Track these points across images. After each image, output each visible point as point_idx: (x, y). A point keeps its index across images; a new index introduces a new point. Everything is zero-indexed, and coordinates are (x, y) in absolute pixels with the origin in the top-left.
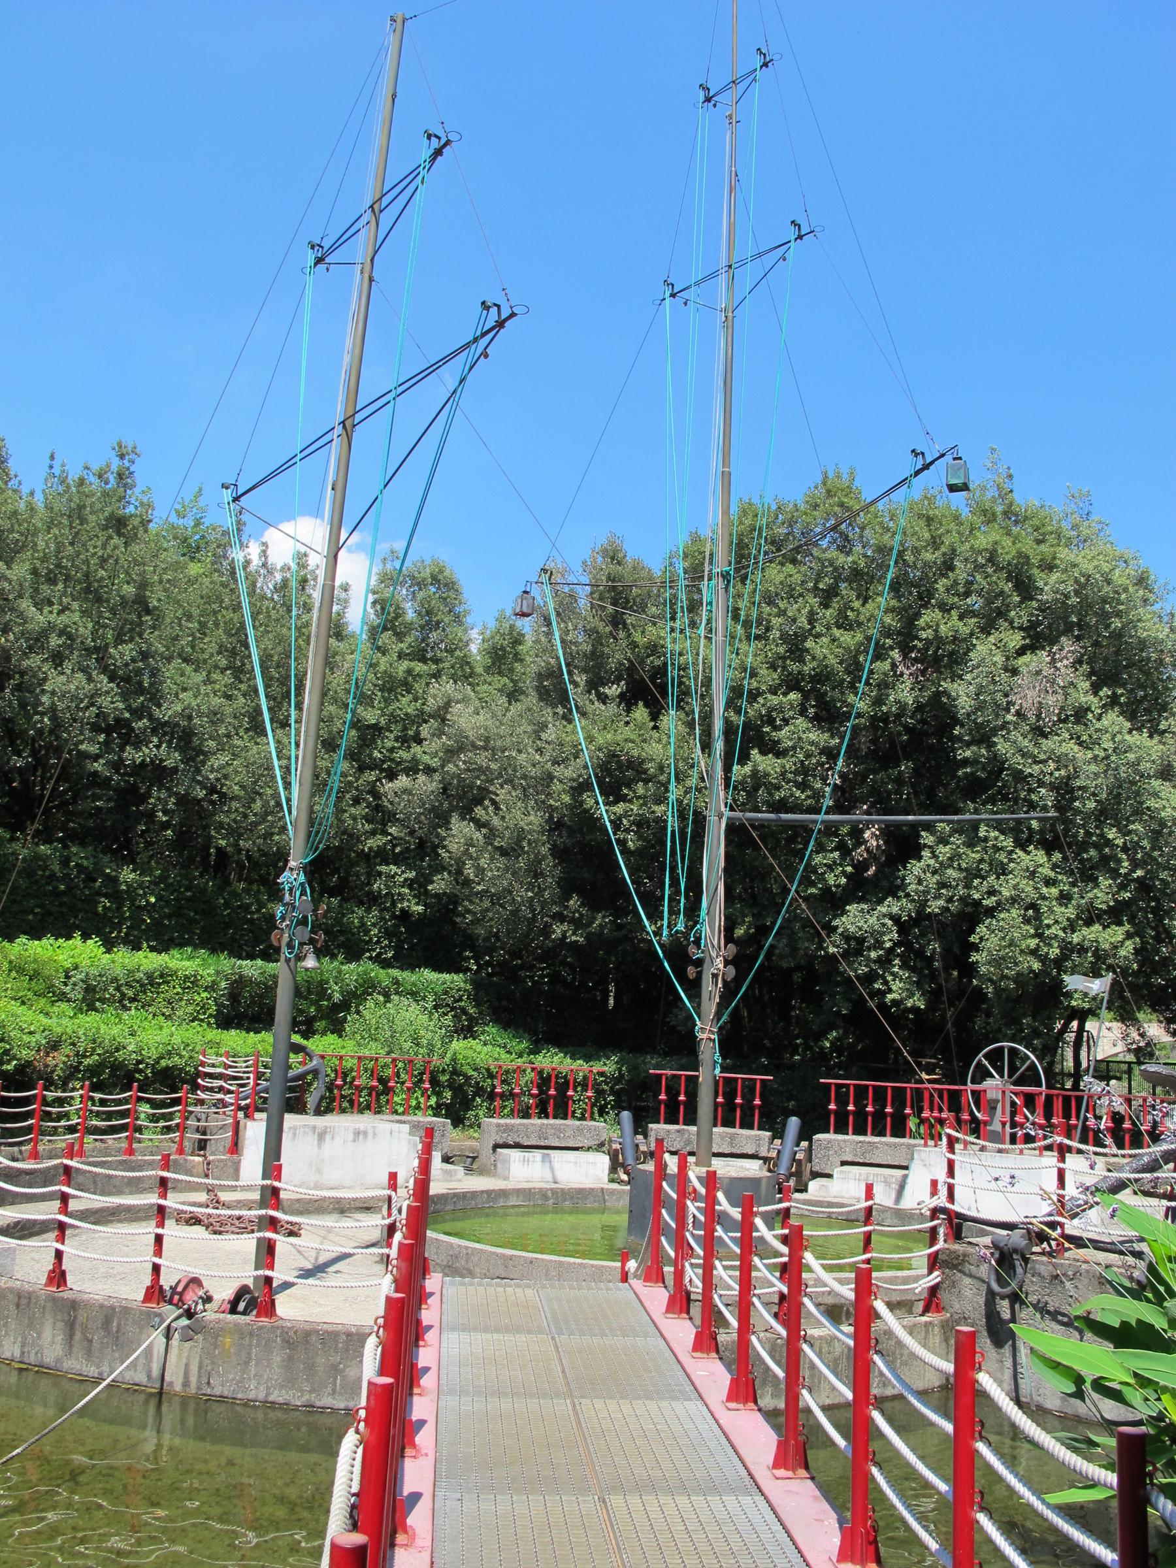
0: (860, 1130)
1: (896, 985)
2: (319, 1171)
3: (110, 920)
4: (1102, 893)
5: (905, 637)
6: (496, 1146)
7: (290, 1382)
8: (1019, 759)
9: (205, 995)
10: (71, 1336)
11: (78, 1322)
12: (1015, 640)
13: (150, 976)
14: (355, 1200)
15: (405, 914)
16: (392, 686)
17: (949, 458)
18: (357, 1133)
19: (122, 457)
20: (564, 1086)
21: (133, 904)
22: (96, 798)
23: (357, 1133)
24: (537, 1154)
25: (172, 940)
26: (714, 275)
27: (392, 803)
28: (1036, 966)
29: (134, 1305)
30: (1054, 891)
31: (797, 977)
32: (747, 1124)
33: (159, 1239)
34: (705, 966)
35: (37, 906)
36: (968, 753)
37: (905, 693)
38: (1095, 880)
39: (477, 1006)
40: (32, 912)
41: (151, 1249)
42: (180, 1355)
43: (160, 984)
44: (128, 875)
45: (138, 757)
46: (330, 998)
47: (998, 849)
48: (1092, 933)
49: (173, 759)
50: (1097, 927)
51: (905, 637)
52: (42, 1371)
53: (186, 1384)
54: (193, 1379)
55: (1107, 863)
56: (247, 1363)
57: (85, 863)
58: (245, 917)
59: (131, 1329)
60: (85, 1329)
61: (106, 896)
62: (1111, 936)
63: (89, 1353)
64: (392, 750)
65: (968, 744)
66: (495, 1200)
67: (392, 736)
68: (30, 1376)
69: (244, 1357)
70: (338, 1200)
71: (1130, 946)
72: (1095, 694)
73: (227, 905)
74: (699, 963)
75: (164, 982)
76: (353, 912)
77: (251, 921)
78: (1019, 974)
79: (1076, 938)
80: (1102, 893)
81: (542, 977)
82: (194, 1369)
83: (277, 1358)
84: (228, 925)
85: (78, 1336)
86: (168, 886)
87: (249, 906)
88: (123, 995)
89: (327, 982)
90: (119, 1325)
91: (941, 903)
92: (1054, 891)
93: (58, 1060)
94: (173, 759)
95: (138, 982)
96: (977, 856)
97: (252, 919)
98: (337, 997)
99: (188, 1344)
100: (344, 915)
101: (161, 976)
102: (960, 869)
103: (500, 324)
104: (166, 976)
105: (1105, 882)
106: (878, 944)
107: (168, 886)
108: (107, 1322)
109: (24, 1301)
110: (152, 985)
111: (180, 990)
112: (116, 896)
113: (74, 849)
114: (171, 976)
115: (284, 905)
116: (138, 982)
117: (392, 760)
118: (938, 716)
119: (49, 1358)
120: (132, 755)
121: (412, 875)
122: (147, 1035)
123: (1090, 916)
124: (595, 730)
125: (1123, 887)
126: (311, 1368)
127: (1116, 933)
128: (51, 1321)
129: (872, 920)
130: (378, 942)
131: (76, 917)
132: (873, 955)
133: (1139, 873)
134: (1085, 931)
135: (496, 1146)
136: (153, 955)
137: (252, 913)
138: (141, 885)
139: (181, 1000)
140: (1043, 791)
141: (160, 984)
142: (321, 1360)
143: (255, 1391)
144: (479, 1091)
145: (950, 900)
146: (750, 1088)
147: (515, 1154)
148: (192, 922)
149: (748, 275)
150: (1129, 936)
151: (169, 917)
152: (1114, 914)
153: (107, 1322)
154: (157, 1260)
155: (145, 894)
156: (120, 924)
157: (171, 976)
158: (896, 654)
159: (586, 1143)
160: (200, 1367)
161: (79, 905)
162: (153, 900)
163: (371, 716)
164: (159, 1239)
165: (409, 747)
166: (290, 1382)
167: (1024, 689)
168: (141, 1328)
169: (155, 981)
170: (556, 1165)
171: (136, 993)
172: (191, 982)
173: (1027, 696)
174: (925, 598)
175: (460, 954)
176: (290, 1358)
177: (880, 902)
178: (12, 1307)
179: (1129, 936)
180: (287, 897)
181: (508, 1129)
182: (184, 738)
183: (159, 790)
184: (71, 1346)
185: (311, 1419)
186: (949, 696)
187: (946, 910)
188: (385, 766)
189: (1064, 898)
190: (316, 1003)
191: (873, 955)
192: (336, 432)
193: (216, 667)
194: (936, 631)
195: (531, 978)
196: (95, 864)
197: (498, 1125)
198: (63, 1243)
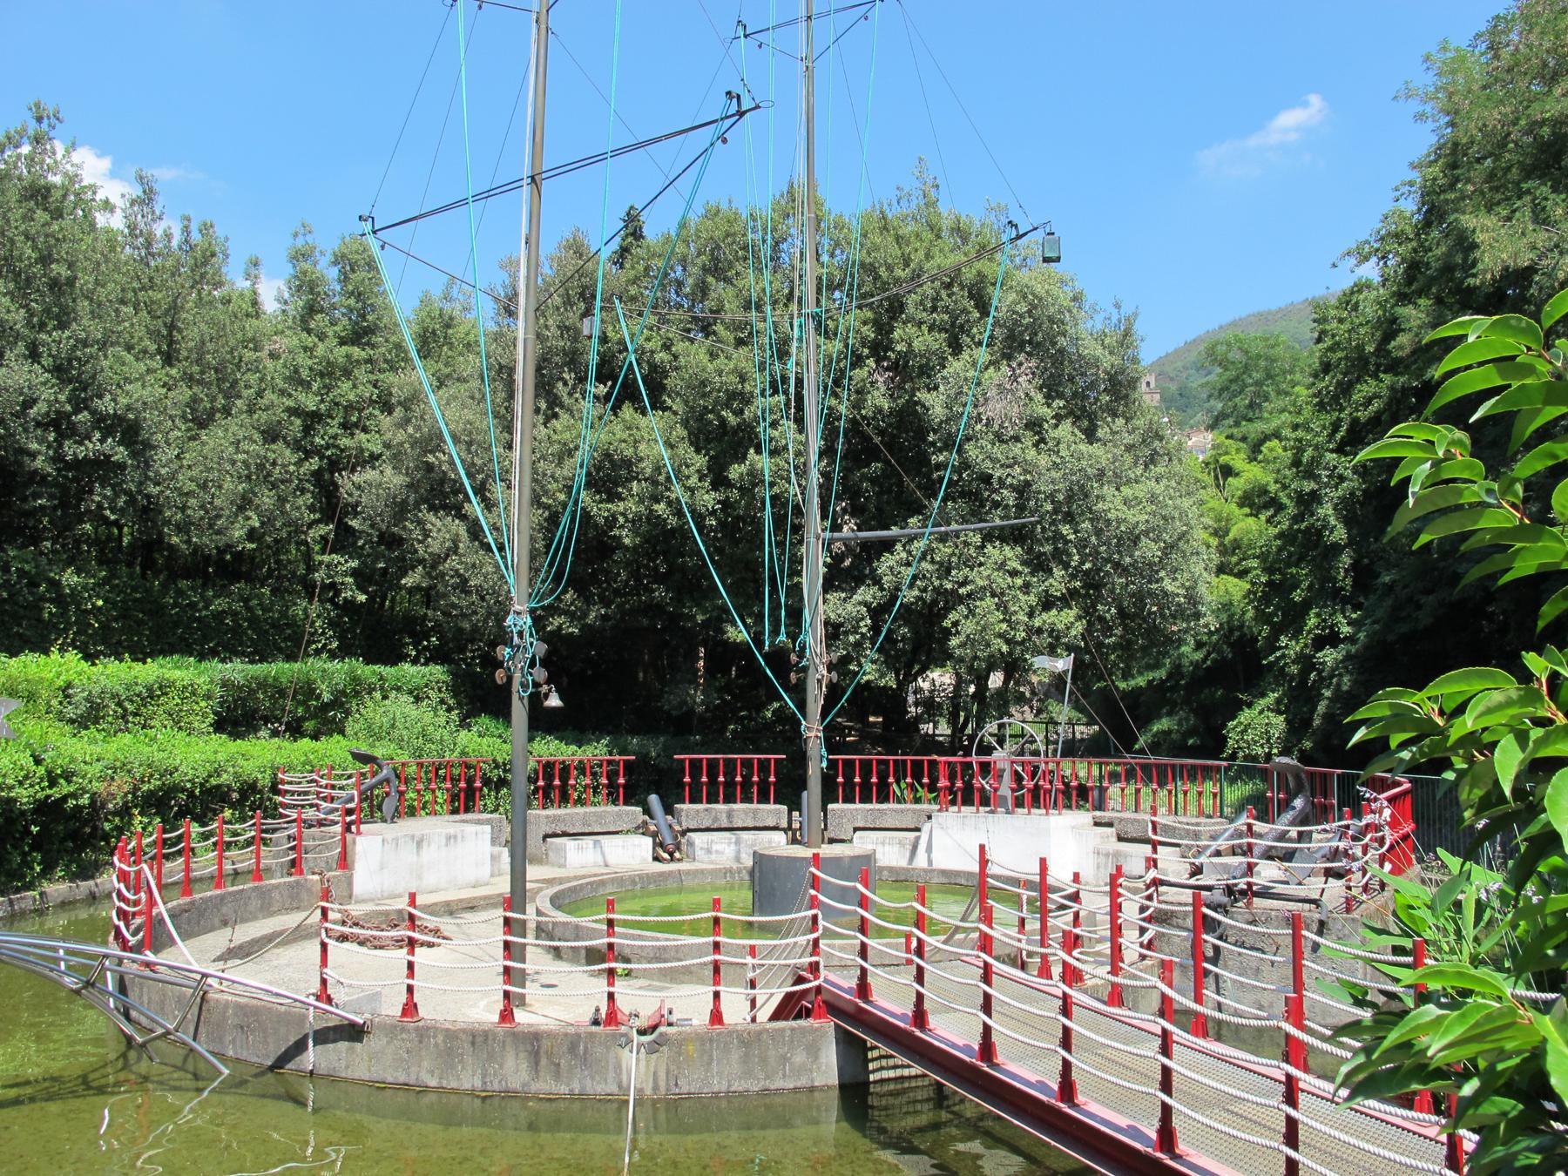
0: (866, 799)
1: (868, 667)
2: (420, 877)
3: (55, 626)
4: (1057, 582)
5: (879, 348)
6: (546, 837)
7: (748, 1074)
8: (988, 463)
9: (203, 704)
10: (537, 1063)
11: (542, 1051)
12: (983, 355)
13: (150, 689)
14: (461, 901)
15: (350, 605)
16: (329, 373)
17: (1040, 232)
18: (449, 838)
19: (39, 120)
20: (565, 771)
21: (78, 608)
22: (37, 496)
23: (449, 838)
24: (589, 840)
25: (119, 643)
26: (794, 22)
27: (350, 495)
28: (1005, 648)
29: (582, 1030)
30: (1019, 582)
32: (764, 798)
33: (411, 965)
34: (811, 671)
36: (941, 458)
37: (879, 399)
38: (1050, 572)
39: (454, 697)
41: (405, 971)
42: (648, 1066)
44: (70, 578)
45: (81, 452)
46: (319, 697)
47: (966, 544)
48: (1050, 617)
49: (121, 454)
50: (1054, 612)
51: (879, 348)
52: (509, 1095)
53: (656, 1088)
54: (662, 1084)
55: (1060, 556)
56: (709, 1064)
57: (27, 567)
59: (598, 1051)
60: (550, 1056)
61: (51, 601)
62: (1066, 619)
63: (557, 1075)
64: (335, 437)
65: (941, 450)
66: (596, 890)
67: (335, 422)
68: (496, 1101)
69: (706, 1058)
70: (447, 903)
71: (1079, 627)
72: (1049, 406)
73: (175, 605)
74: (805, 669)
77: (199, 620)
78: (992, 656)
79: (1037, 623)
80: (1057, 582)
81: (473, 658)
82: (662, 1075)
83: (735, 1056)
84: (176, 625)
85: (544, 1061)
86: (113, 587)
88: (125, 710)
89: (314, 682)
90: (586, 1048)
91: (916, 593)
92: (1019, 582)
93: (119, 789)
94: (121, 454)
96: (949, 551)
98: (326, 697)
99: (654, 1056)
100: (288, 608)
101: (160, 688)
102: (933, 561)
103: (741, 114)
104: (164, 687)
105: (1058, 572)
106: (855, 630)
107: (113, 587)
108: (573, 1048)
109: (479, 1040)
112: (60, 600)
115: (512, 647)
117: (337, 447)
118: (909, 420)
119: (515, 1083)
120: (71, 450)
121: (354, 564)
122: (197, 753)
123: (1047, 603)
124: (589, 428)
125: (1073, 577)
126: (764, 1060)
127: (1069, 615)
128: (512, 1053)
129: (849, 607)
130: (323, 633)
131: (20, 625)
132: (852, 639)
133: (1088, 566)
134: (1045, 616)
135: (546, 837)
136: (138, 666)
138: (85, 588)
140: (1005, 492)
142: (772, 1053)
143: (719, 1085)
144: (487, 782)
145: (924, 590)
146: (764, 767)
147: (569, 844)
148: (140, 623)
149: (825, 30)
150: (1079, 618)
151: (116, 620)
152: (1065, 601)
153: (573, 1048)
154: (410, 981)
155: (90, 597)
156: (66, 630)
158: (871, 362)
159: (625, 827)
160: (668, 1073)
161: (22, 611)
162: (100, 603)
163: (310, 402)
164: (411, 965)
165: (352, 435)
166: (748, 1074)
167: (982, 396)
168: (608, 1048)
169: (155, 693)
170: (606, 850)
171: (132, 710)
172: (189, 692)
173: (995, 408)
174: (896, 308)
175: (400, 640)
176: (746, 1055)
177: (853, 591)
178: (467, 1046)
179: (1079, 618)
180: (516, 640)
181: (556, 819)
182: (128, 430)
183: (103, 487)
184: (537, 1071)
185: (767, 1101)
186: (923, 406)
187: (919, 598)
188: (329, 453)
189: (1026, 587)
190: (304, 703)
191: (852, 639)
192: (524, 182)
193: (145, 352)
194: (910, 345)
195: (464, 660)
196: (37, 567)
197: (547, 817)
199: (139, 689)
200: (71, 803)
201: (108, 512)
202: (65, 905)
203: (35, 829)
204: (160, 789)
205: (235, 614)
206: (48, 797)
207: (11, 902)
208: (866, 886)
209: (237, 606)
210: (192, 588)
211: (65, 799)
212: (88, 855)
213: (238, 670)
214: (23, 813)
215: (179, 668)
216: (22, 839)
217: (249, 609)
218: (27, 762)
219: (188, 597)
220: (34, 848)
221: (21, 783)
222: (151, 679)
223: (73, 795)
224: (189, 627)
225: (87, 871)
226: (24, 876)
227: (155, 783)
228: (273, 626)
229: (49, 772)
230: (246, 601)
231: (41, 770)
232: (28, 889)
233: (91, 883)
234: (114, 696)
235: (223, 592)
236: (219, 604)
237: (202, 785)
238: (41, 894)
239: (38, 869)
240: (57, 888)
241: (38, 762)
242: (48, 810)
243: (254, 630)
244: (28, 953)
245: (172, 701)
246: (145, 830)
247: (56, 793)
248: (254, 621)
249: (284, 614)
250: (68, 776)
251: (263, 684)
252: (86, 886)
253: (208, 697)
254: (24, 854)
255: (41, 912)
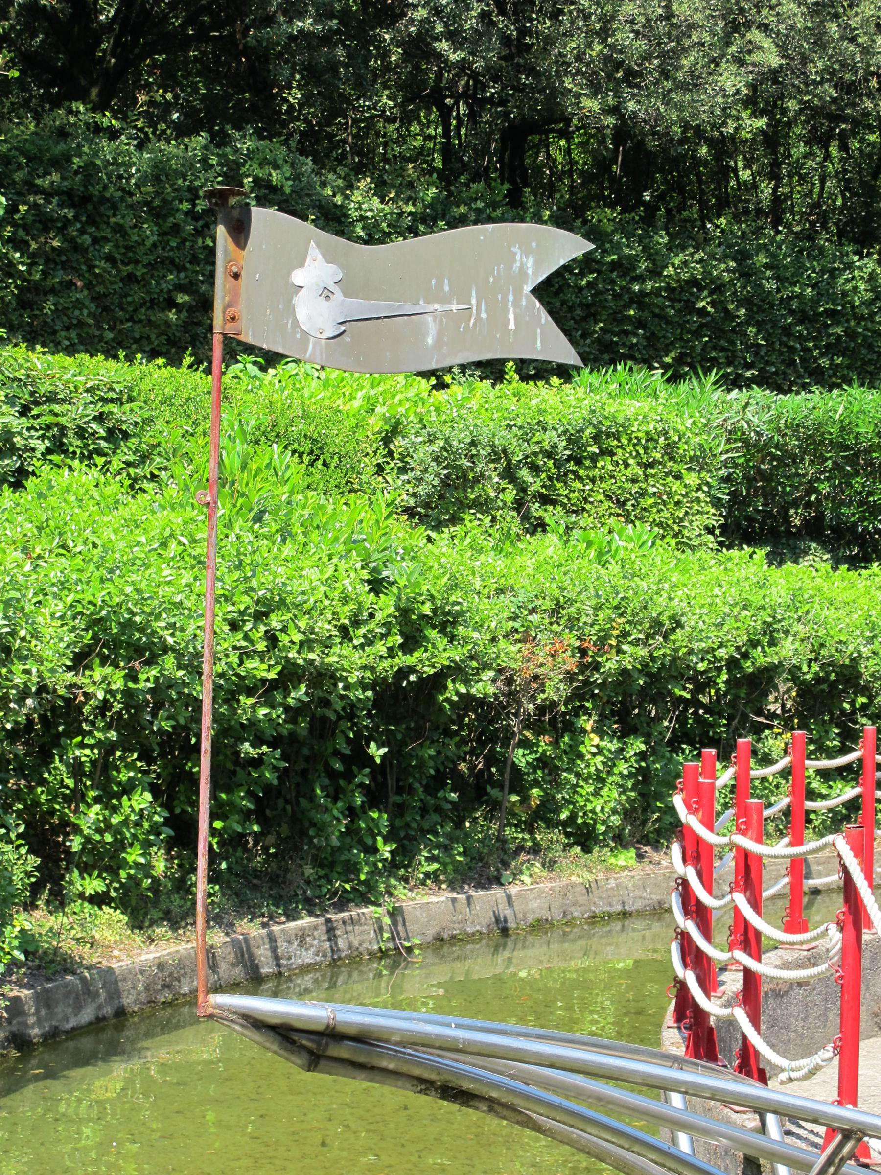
9: (692, 479)
31: (114, 802)
35: (180, 288)
40: (171, 303)
43: (594, 458)
57: (276, 177)
58: (627, 289)
75: (603, 453)
76: (850, 266)
77: (639, 300)
87: (633, 261)
95: (549, 455)
97: (642, 293)
100: (834, 273)
101: (596, 438)
110: (579, 462)
111: (639, 471)
113: (246, 145)
114: (617, 436)
116: (549, 455)
137: (640, 279)
139: (643, 494)
141: (594, 458)
157: (617, 436)
169: (584, 449)
172: (662, 452)
196: (296, 177)
198: (759, 959)
199: (549, 438)
200: (454, 689)
201: (443, 46)
202: (442, 943)
203: (377, 752)
204: (645, 669)
205: (718, 288)
206: (403, 672)
207: (331, 930)
208: (755, 1021)
209: (724, 270)
210: (621, 227)
211: (438, 681)
212: (480, 826)
213: (761, 410)
214: (351, 710)
215: (632, 394)
216: (349, 776)
217: (746, 273)
218: (353, 581)
219: (617, 247)
220: (375, 799)
221: (345, 633)
222: (577, 418)
223: (455, 671)
224: (617, 318)
225: (483, 869)
226: (352, 869)
227: (632, 655)
228: (803, 318)
229: (404, 612)
230: (743, 257)
231: (386, 607)
232: (365, 901)
233: (496, 893)
234: (498, 454)
235: (686, 235)
236: (682, 265)
237: (733, 664)
238: (394, 914)
239: (386, 850)
240: (425, 904)
241: (377, 585)
242: (405, 701)
243: (759, 325)
244: (579, 1094)
245: (621, 472)
246: (602, 769)
247: (423, 661)
248: (759, 306)
249: (822, 290)
250: (447, 622)
251: (814, 442)
252: (486, 901)
253: (699, 462)
254: (352, 812)
255: (395, 956)
